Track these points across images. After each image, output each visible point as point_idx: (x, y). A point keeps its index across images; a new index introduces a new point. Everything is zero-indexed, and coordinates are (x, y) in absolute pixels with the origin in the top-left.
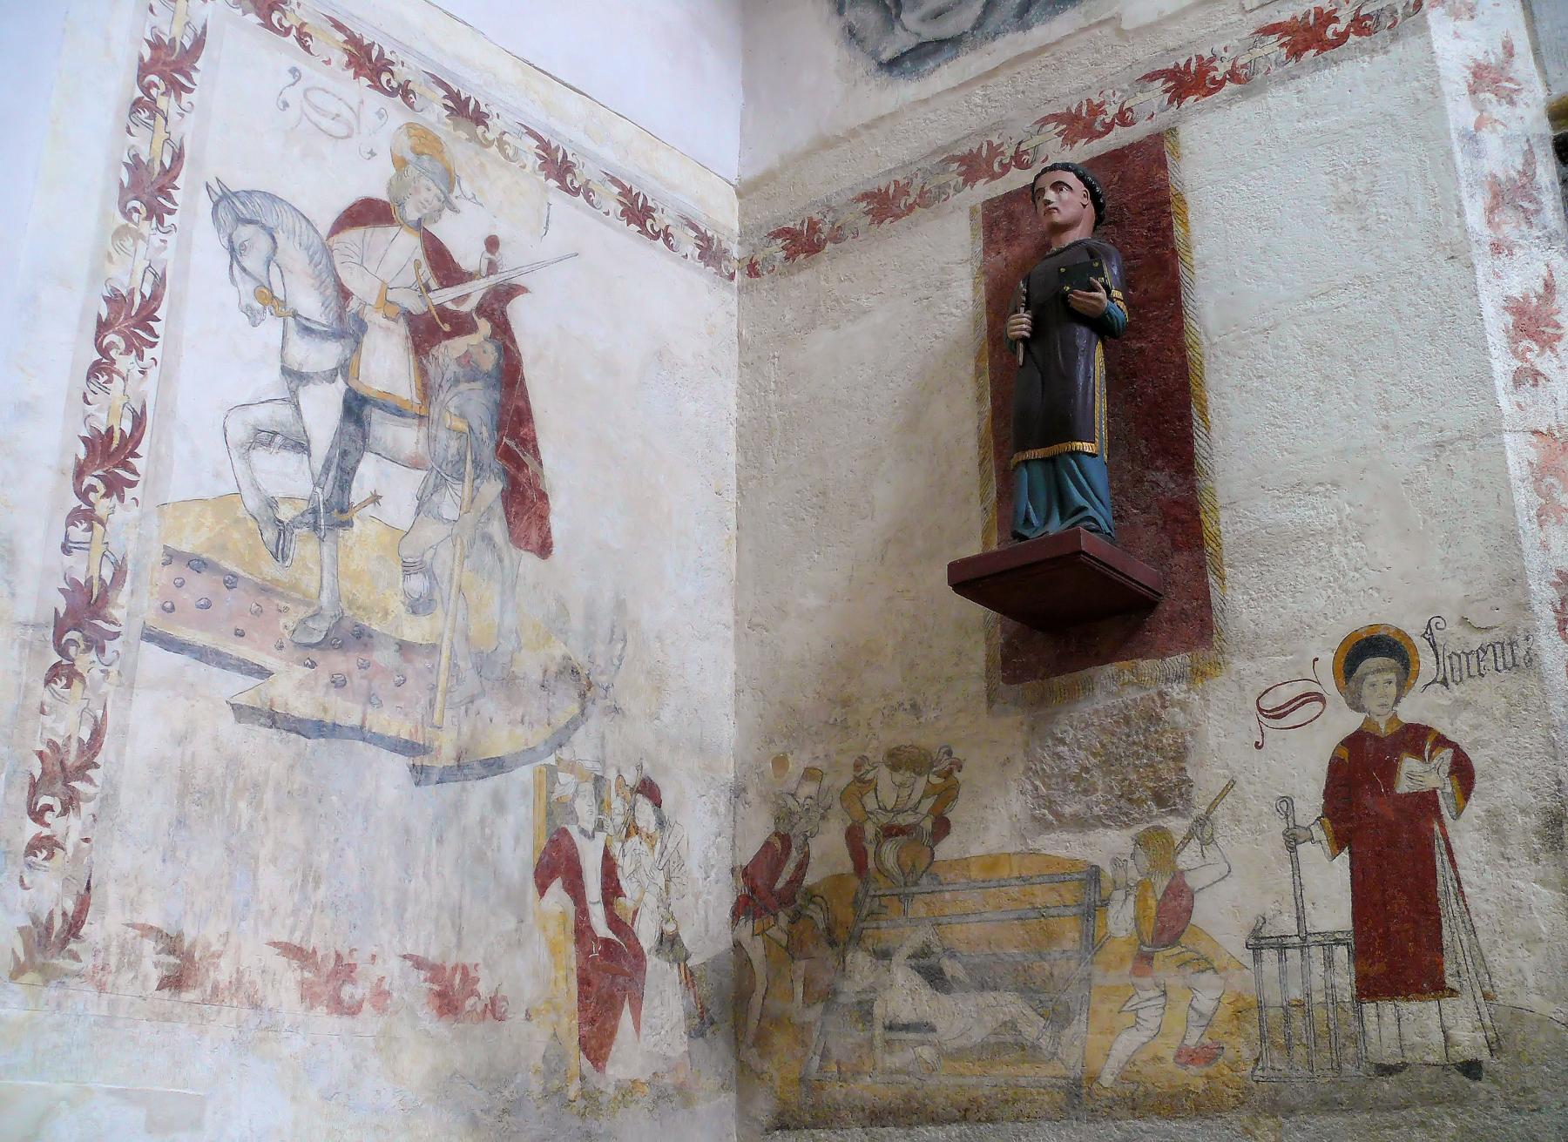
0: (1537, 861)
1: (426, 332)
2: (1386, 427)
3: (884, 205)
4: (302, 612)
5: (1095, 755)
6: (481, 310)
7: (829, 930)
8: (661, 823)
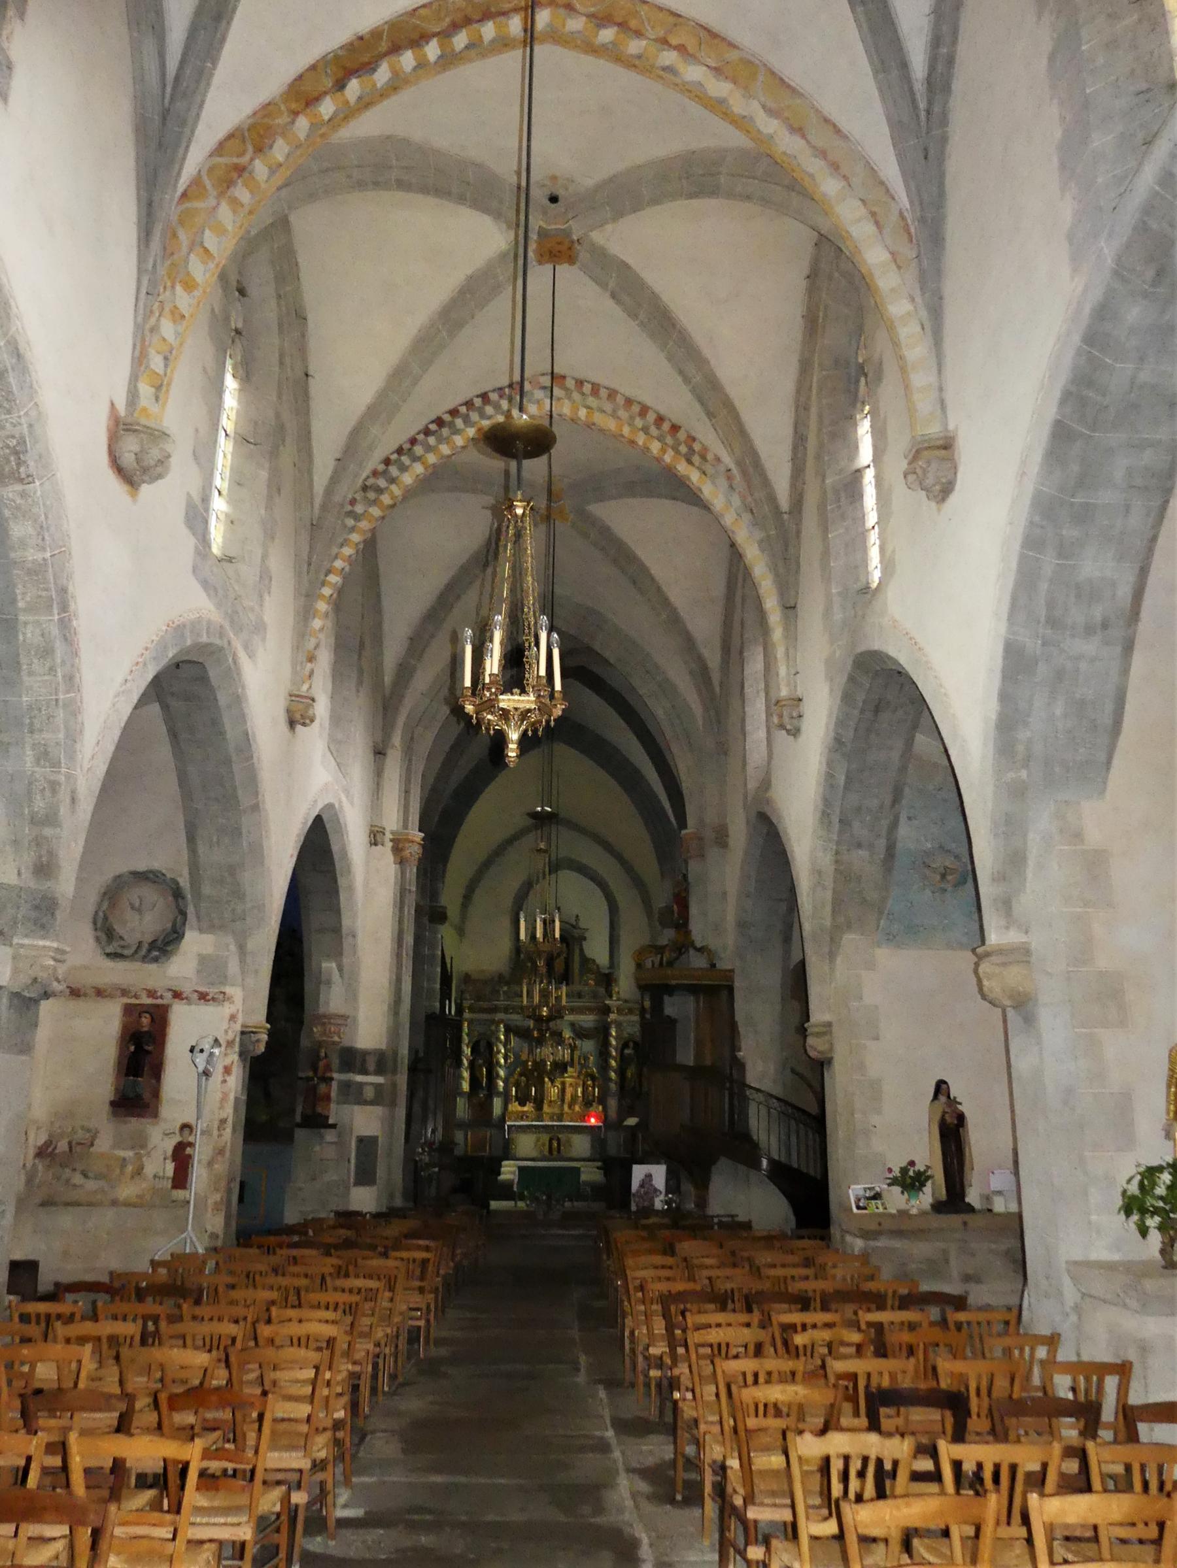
3: (100, 993)
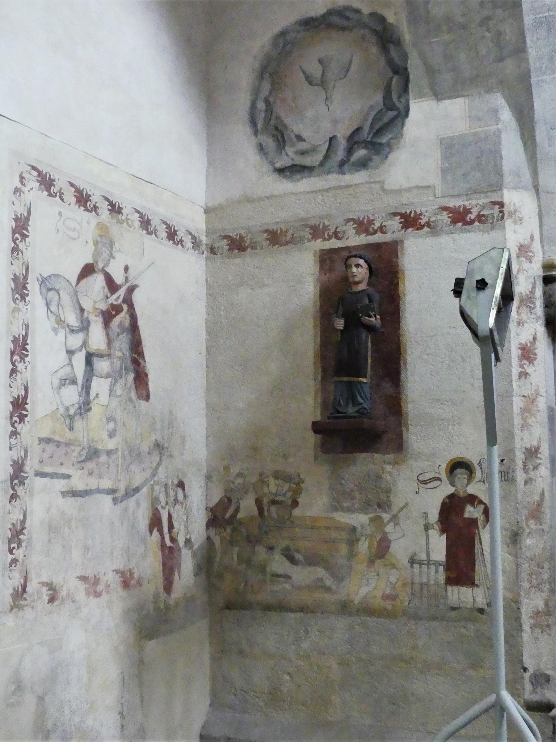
0: (508, 547)
1: (108, 317)
2: (472, 385)
3: (275, 238)
4: (78, 449)
5: (356, 486)
6: (124, 301)
7: (248, 536)
8: (185, 496)
